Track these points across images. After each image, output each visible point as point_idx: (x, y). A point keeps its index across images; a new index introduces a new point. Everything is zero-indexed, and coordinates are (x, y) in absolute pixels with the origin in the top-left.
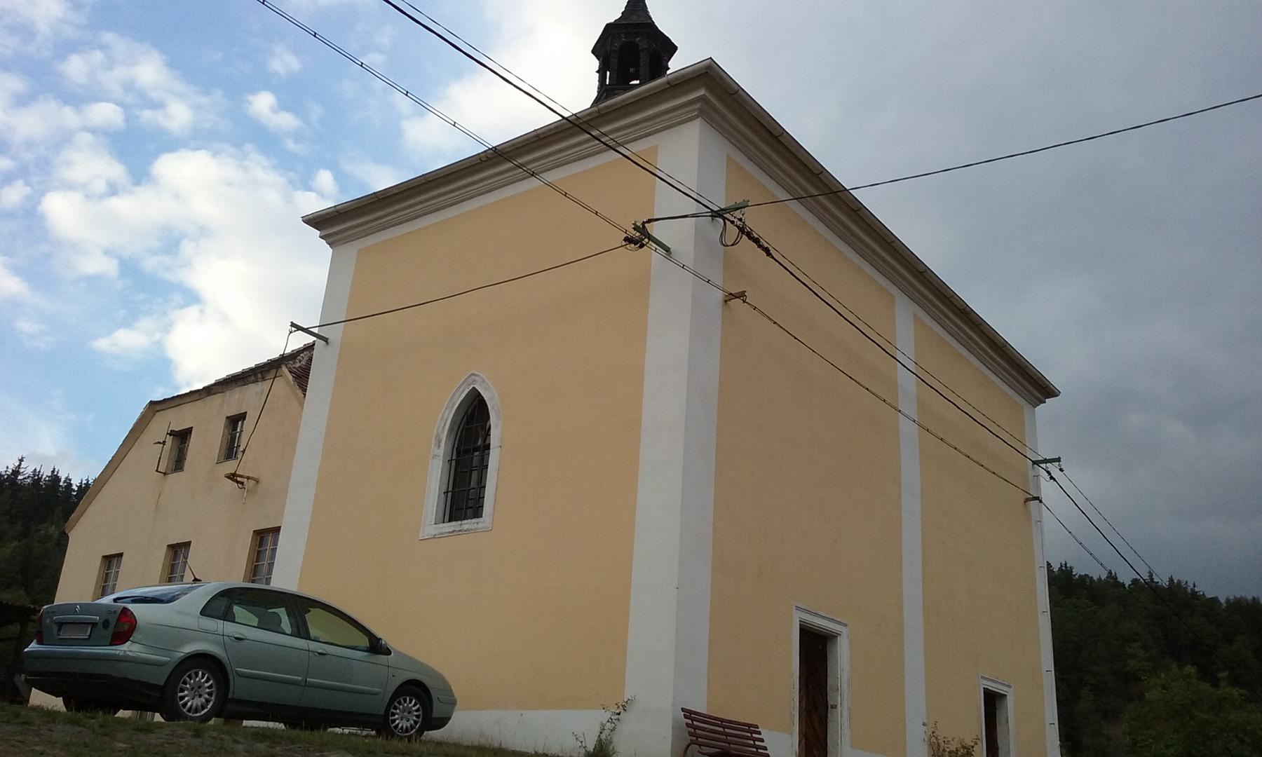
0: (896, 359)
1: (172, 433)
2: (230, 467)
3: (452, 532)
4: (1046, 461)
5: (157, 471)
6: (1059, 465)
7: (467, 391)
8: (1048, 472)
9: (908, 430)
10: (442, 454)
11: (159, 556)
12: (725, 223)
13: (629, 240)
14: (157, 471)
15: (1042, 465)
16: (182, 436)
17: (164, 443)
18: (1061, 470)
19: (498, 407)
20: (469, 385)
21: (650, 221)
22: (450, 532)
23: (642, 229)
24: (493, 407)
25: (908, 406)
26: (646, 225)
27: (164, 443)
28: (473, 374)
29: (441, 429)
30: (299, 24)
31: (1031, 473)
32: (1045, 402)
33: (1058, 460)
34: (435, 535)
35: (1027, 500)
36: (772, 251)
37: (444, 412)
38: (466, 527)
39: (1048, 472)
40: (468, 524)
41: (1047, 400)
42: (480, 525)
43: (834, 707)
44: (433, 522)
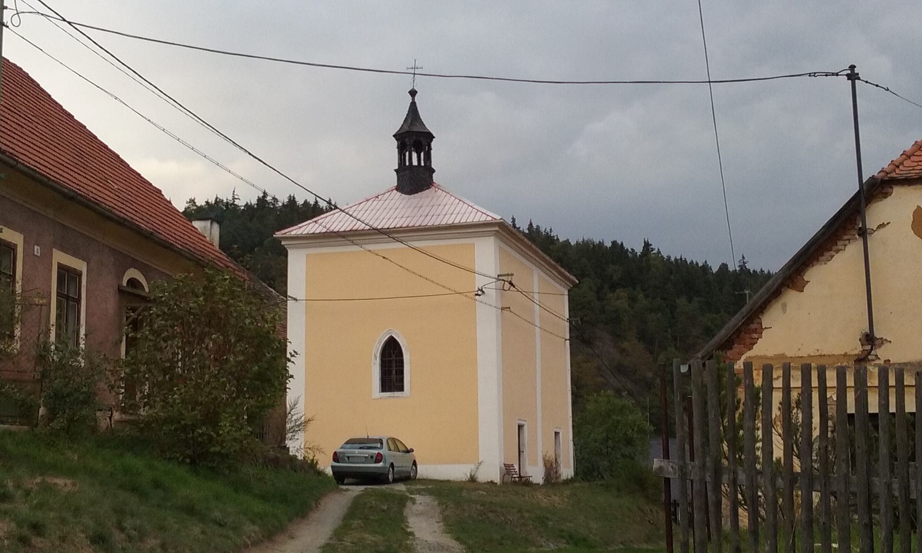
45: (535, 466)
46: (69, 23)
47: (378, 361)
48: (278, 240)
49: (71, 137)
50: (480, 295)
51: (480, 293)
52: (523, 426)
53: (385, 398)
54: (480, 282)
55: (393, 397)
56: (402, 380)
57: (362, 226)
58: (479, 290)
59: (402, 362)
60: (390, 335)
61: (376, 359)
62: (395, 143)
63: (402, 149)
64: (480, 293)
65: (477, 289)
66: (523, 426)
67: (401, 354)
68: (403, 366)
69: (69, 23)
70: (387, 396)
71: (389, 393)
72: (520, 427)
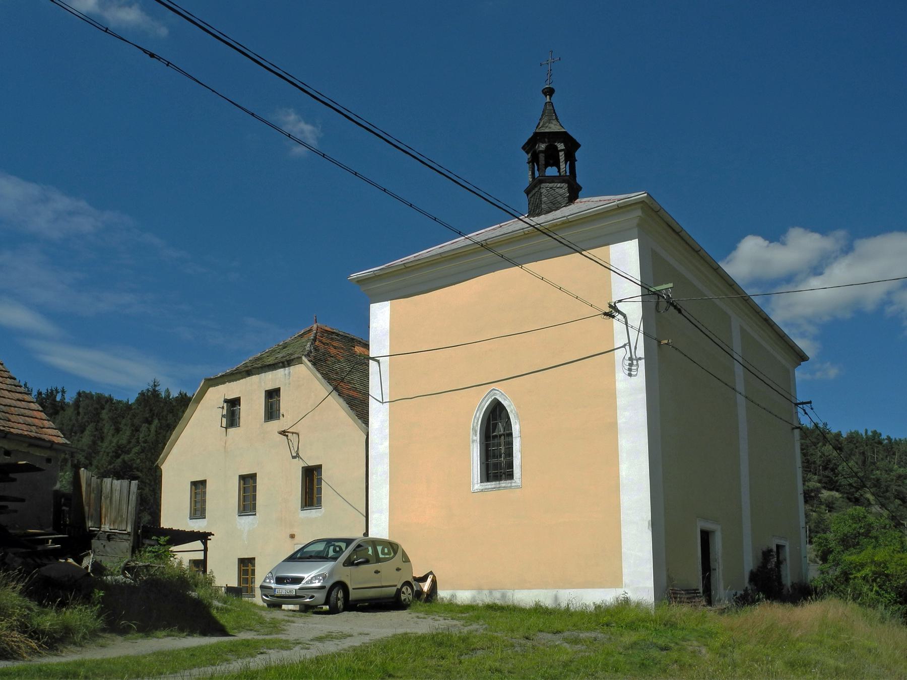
0: (743, 366)
1: (226, 401)
2: (275, 426)
3: (494, 488)
4: (803, 403)
5: (221, 426)
6: (811, 406)
7: (490, 400)
8: (804, 410)
9: (741, 400)
10: (478, 440)
11: (234, 486)
12: (658, 297)
13: (606, 314)
14: (221, 426)
15: (801, 406)
16: (233, 403)
17: (223, 408)
18: (812, 409)
19: (515, 411)
20: (492, 396)
21: (620, 301)
22: (491, 488)
23: (614, 307)
24: (511, 411)
25: (740, 387)
26: (616, 304)
27: (223, 408)
28: (494, 389)
29: (475, 424)
30: (537, 276)
31: (794, 411)
32: (800, 365)
33: (810, 402)
34: (482, 489)
35: (793, 429)
36: (683, 311)
37: (476, 413)
38: (503, 485)
39: (804, 410)
40: (503, 483)
41: (802, 363)
42: (513, 484)
43: (715, 570)
44: (479, 482)
55: (499, 487)
56: (510, 465)
60: (493, 398)
61: (476, 435)
68: (512, 467)
70: (490, 487)
71: (494, 483)
72: (706, 537)
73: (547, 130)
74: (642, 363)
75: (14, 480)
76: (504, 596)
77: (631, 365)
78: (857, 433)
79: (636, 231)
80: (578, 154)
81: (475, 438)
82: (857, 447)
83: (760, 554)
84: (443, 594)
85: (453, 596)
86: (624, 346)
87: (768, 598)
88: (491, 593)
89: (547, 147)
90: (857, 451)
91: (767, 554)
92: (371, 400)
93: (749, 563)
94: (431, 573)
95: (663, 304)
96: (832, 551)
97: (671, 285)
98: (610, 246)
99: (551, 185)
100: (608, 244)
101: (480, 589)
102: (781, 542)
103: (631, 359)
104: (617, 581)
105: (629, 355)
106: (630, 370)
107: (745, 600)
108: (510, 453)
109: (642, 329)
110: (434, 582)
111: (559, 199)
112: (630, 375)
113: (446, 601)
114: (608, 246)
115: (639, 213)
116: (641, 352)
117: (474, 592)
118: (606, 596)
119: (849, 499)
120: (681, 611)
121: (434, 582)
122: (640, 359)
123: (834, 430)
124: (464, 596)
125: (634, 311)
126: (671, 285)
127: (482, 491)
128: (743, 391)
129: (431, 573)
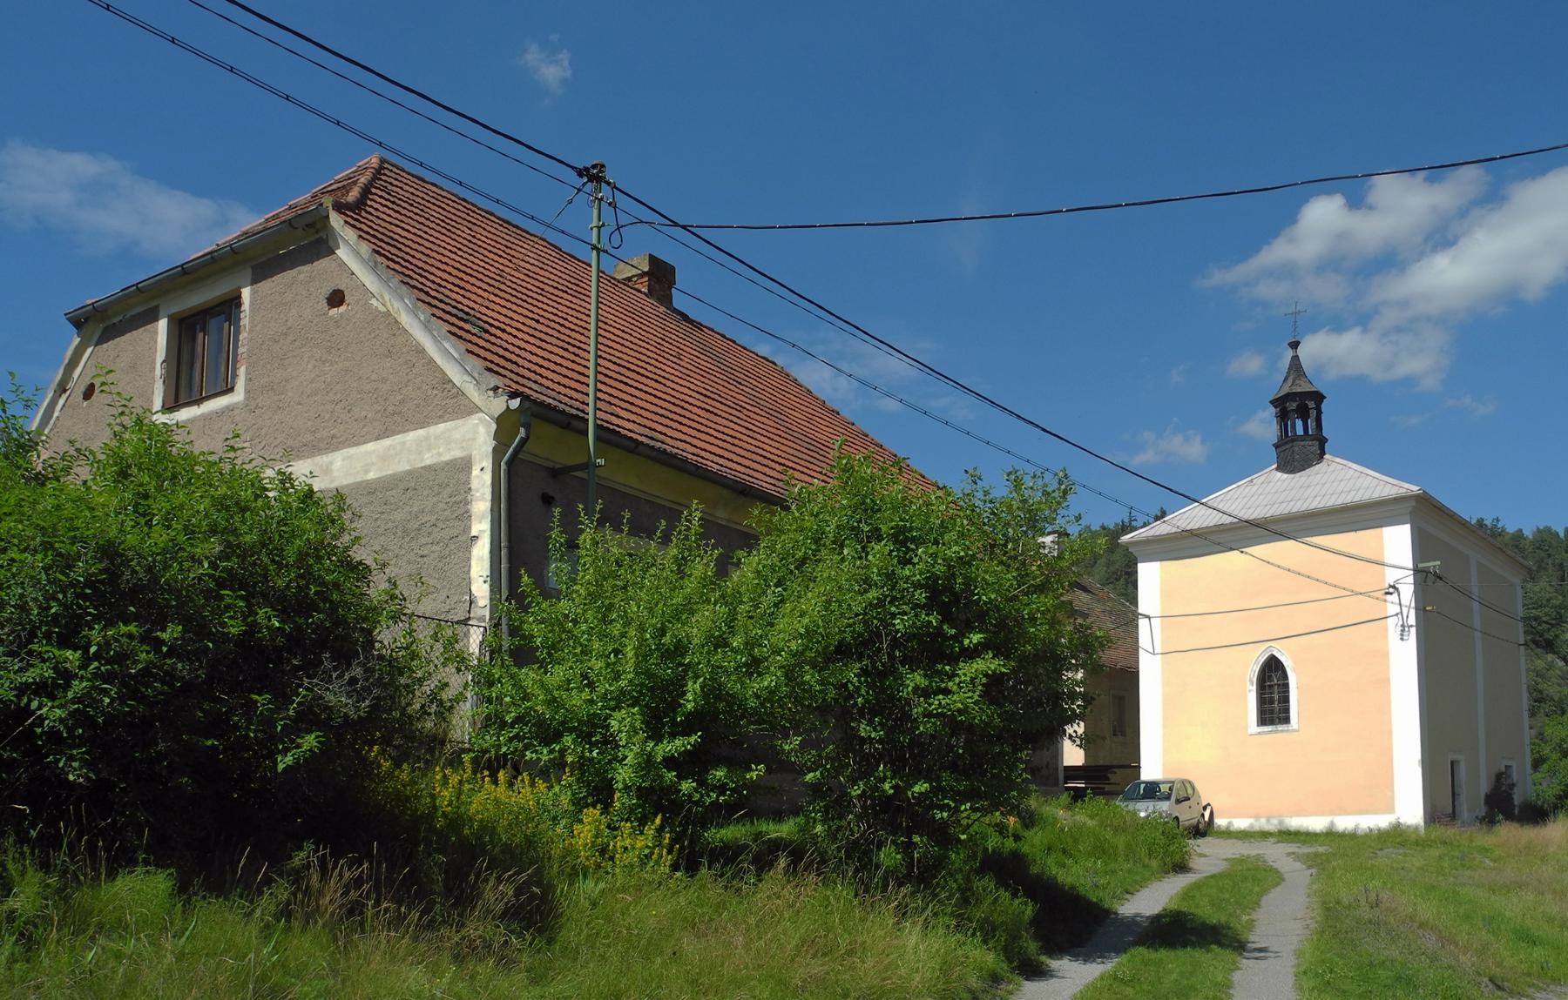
9: (1478, 635)
25: (1477, 623)
40: (1280, 727)
45: (1278, 884)
46: (684, 227)
47: (1254, 688)
48: (1126, 547)
49: (574, 346)
50: (1391, 594)
51: (1391, 590)
52: (1458, 762)
53: (1264, 733)
54: (1391, 576)
56: (1287, 710)
57: (1228, 520)
58: (1390, 586)
59: (1287, 686)
62: (1272, 410)
63: (1283, 416)
64: (1391, 590)
65: (1387, 586)
66: (1458, 762)
67: (1285, 676)
69: (684, 227)
73: (1299, 390)
74: (1413, 630)
75: (1115, 773)
76: (1281, 823)
77: (1403, 631)
78: (1548, 530)
79: (1408, 517)
80: (1324, 407)
81: (1251, 688)
82: (1549, 555)
83: (1493, 776)
84: (1220, 822)
85: (1230, 823)
86: (1397, 615)
87: (1506, 819)
88: (1268, 821)
89: (1298, 406)
90: (1550, 561)
91: (1499, 776)
92: (1142, 653)
93: (1485, 787)
94: (1209, 804)
95: (1431, 577)
96: (1547, 759)
97: (1439, 563)
98: (1384, 529)
99: (1303, 443)
100: (1381, 527)
101: (1257, 817)
102: (1509, 763)
103: (1403, 626)
104: (1390, 809)
105: (1401, 623)
106: (1402, 635)
107: (1489, 820)
108: (1286, 700)
109: (1413, 605)
110: (1212, 814)
111: (1311, 456)
112: (1402, 639)
113: (1223, 829)
114: (1379, 530)
115: (1413, 504)
116: (1412, 620)
117: (1252, 820)
118: (1382, 821)
119: (1535, 642)
120: (1442, 831)
121: (1212, 814)
122: (1412, 626)
123: (1511, 529)
124: (1241, 824)
125: (1407, 591)
126: (1439, 563)
127: (1259, 733)
128: (1479, 628)
129: (1209, 804)
